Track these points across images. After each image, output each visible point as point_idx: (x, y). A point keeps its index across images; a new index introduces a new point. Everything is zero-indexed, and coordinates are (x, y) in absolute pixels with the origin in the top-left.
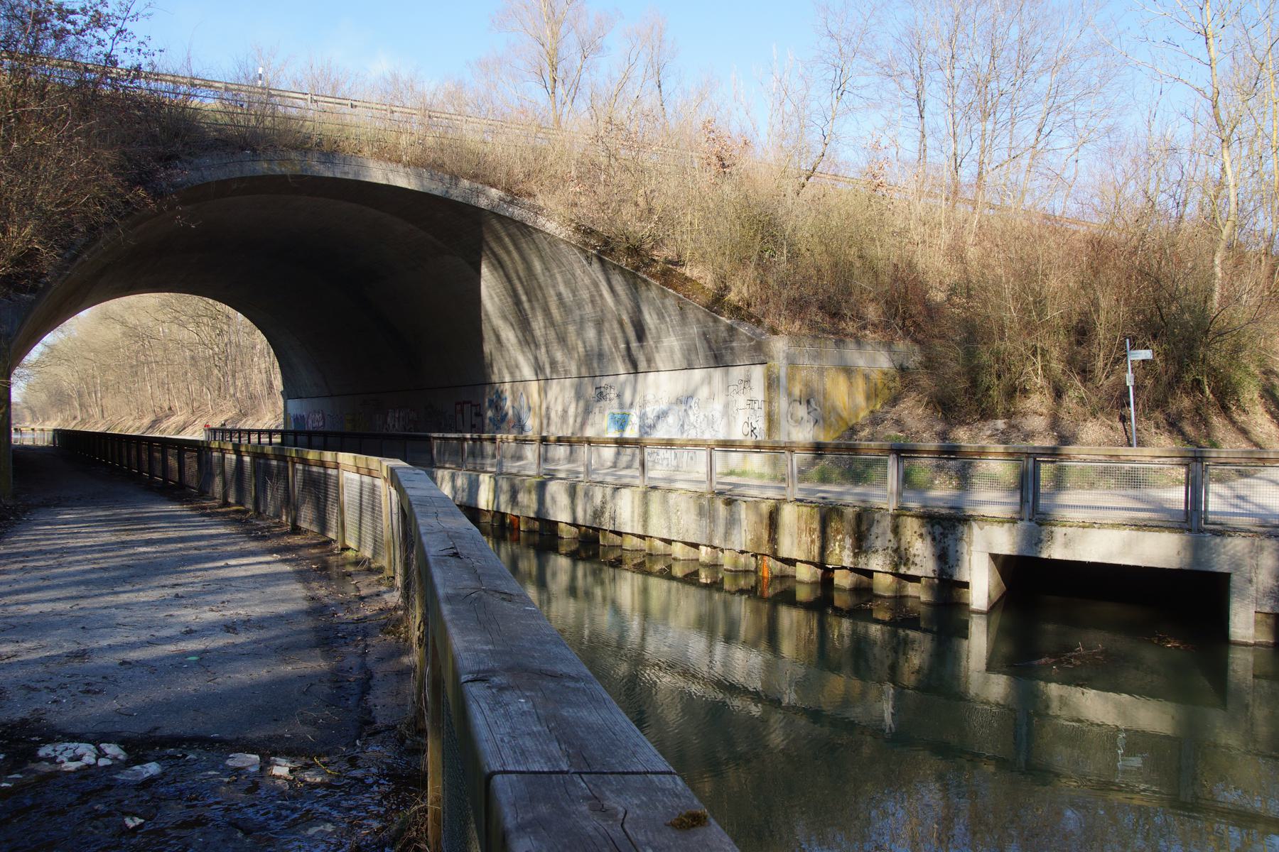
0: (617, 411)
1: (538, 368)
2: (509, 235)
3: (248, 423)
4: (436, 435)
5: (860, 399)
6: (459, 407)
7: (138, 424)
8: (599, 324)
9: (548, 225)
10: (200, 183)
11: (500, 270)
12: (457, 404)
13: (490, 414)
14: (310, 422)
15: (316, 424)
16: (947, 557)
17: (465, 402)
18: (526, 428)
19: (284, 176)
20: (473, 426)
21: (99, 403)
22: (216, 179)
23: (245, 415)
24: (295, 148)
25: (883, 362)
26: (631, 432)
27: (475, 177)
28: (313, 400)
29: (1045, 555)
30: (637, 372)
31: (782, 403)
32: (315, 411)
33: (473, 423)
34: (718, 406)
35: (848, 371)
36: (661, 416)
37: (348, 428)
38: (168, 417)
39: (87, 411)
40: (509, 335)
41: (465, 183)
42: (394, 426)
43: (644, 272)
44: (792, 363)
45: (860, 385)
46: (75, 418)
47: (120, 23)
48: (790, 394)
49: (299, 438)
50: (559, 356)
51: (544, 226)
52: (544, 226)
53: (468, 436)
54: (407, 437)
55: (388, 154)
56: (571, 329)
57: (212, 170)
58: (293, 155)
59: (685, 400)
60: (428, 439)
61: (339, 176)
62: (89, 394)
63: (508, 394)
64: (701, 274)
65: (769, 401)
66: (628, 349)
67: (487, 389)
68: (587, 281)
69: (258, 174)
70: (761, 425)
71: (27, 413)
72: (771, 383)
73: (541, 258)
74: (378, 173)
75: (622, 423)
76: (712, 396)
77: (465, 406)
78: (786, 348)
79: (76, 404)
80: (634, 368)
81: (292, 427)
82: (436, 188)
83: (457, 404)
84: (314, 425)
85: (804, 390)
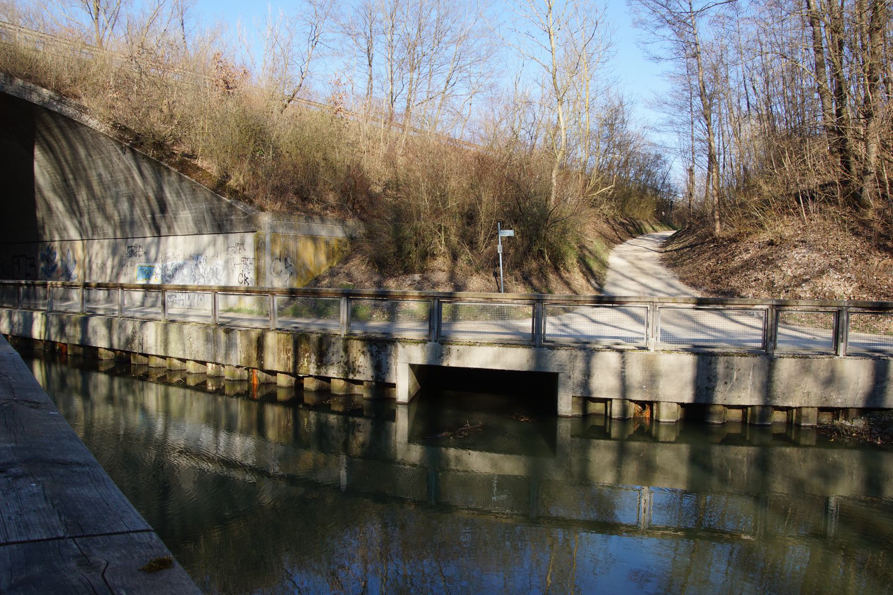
1: (82, 231)
5: (323, 258)
8: (131, 200)
9: (91, 121)
13: (42, 265)
16: (381, 367)
27: (28, 78)
29: (445, 364)
31: (267, 260)
35: (314, 239)
36: (178, 268)
40: (58, 205)
51: (87, 122)
52: (87, 122)
53: (23, 282)
56: (109, 202)
65: (257, 259)
66: (153, 218)
68: (122, 166)
70: (251, 276)
72: (259, 247)
75: (148, 273)
78: (270, 221)
80: (158, 232)
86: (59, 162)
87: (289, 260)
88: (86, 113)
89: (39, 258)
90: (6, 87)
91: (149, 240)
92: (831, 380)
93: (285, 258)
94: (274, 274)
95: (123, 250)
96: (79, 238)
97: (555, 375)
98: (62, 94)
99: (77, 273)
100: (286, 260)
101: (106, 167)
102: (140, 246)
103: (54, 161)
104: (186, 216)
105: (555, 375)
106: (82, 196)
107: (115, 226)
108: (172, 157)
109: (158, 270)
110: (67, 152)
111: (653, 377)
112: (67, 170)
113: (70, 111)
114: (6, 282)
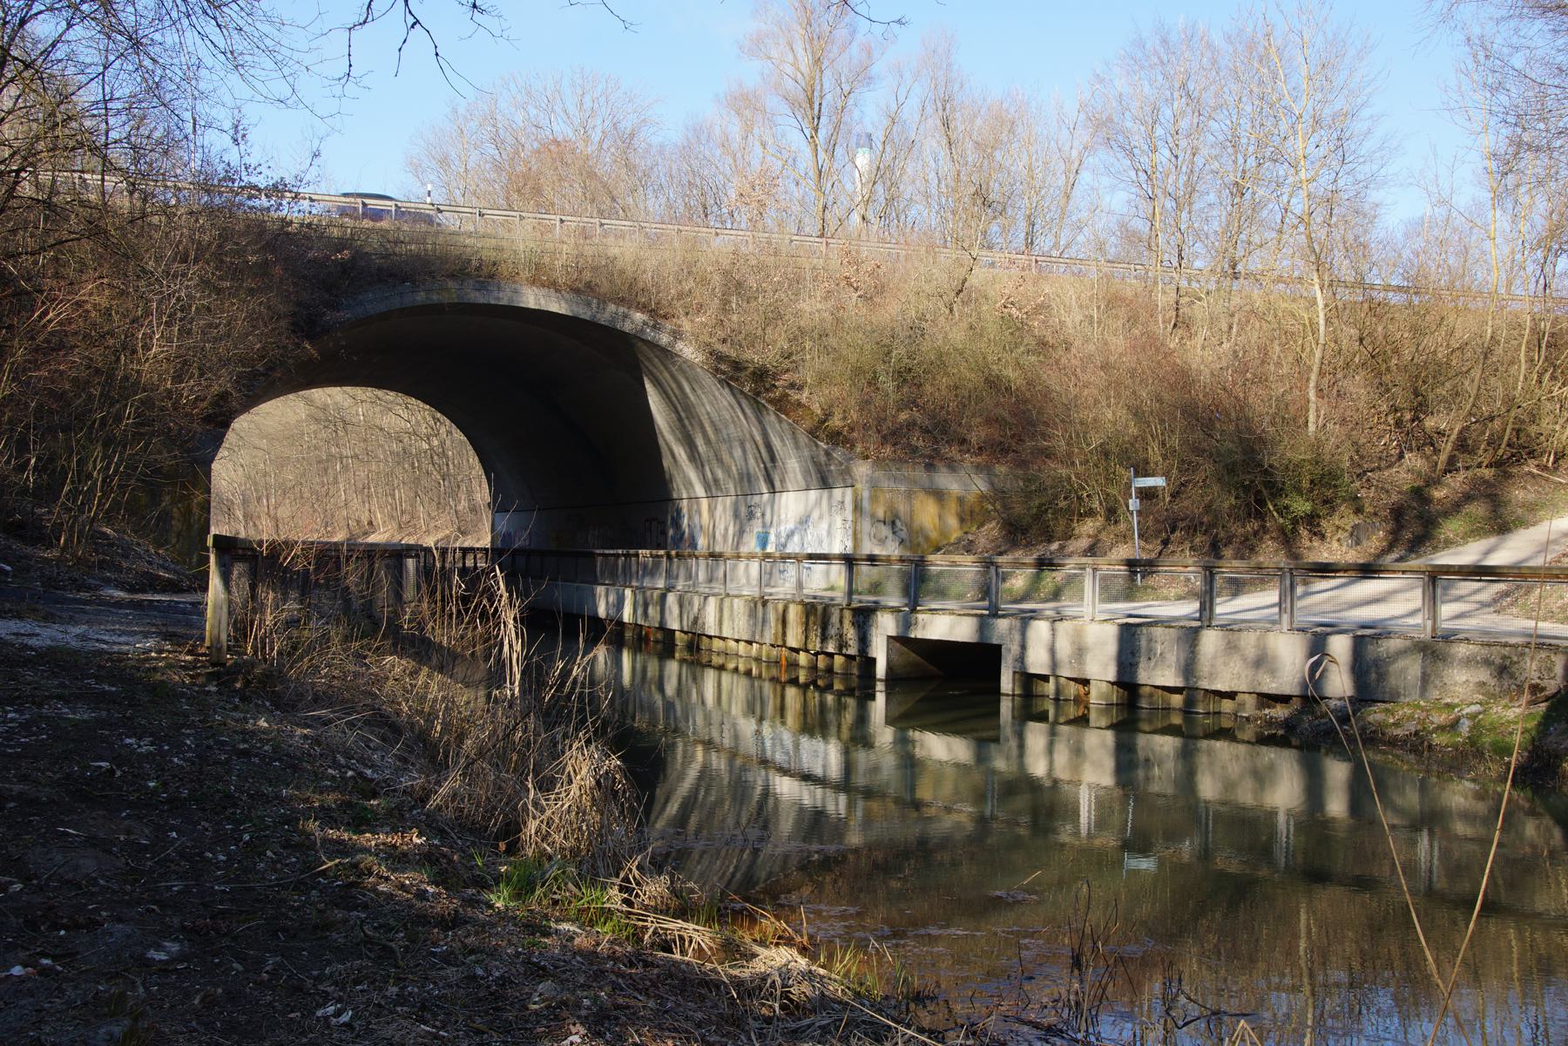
0: (760, 529)
1: (707, 487)
2: (657, 357)
4: (598, 551)
5: (953, 522)
9: (685, 349)
13: (671, 532)
16: (864, 641)
19: (442, 305)
21: (272, 513)
24: (452, 276)
25: (980, 485)
27: (622, 301)
29: (913, 636)
31: (866, 525)
34: (824, 525)
35: (939, 495)
36: (790, 535)
39: (255, 525)
40: (681, 452)
41: (612, 307)
44: (874, 486)
45: (953, 506)
47: (295, 190)
48: (873, 516)
50: (720, 474)
53: (620, 551)
55: (541, 277)
56: (724, 447)
57: (375, 302)
58: (451, 284)
59: (804, 521)
60: (593, 555)
61: (493, 302)
62: (259, 499)
63: (685, 511)
64: (813, 400)
65: (855, 522)
66: (766, 468)
67: (670, 504)
68: (726, 403)
70: (850, 544)
72: (857, 508)
73: (687, 379)
74: (532, 299)
75: (764, 542)
76: (821, 517)
78: (870, 472)
79: (240, 514)
80: (773, 490)
81: (499, 544)
82: (584, 313)
85: (888, 514)
86: (665, 392)
87: (898, 523)
90: (598, 316)
91: (766, 496)
92: (1262, 661)
93: (892, 522)
94: (875, 541)
96: (704, 495)
97: (999, 647)
98: (657, 314)
99: (702, 542)
100: (893, 523)
101: (711, 404)
104: (793, 465)
105: (999, 647)
108: (772, 391)
109: (772, 538)
110: (674, 386)
111: (1080, 652)
112: (680, 409)
113: (664, 339)
114: (607, 552)
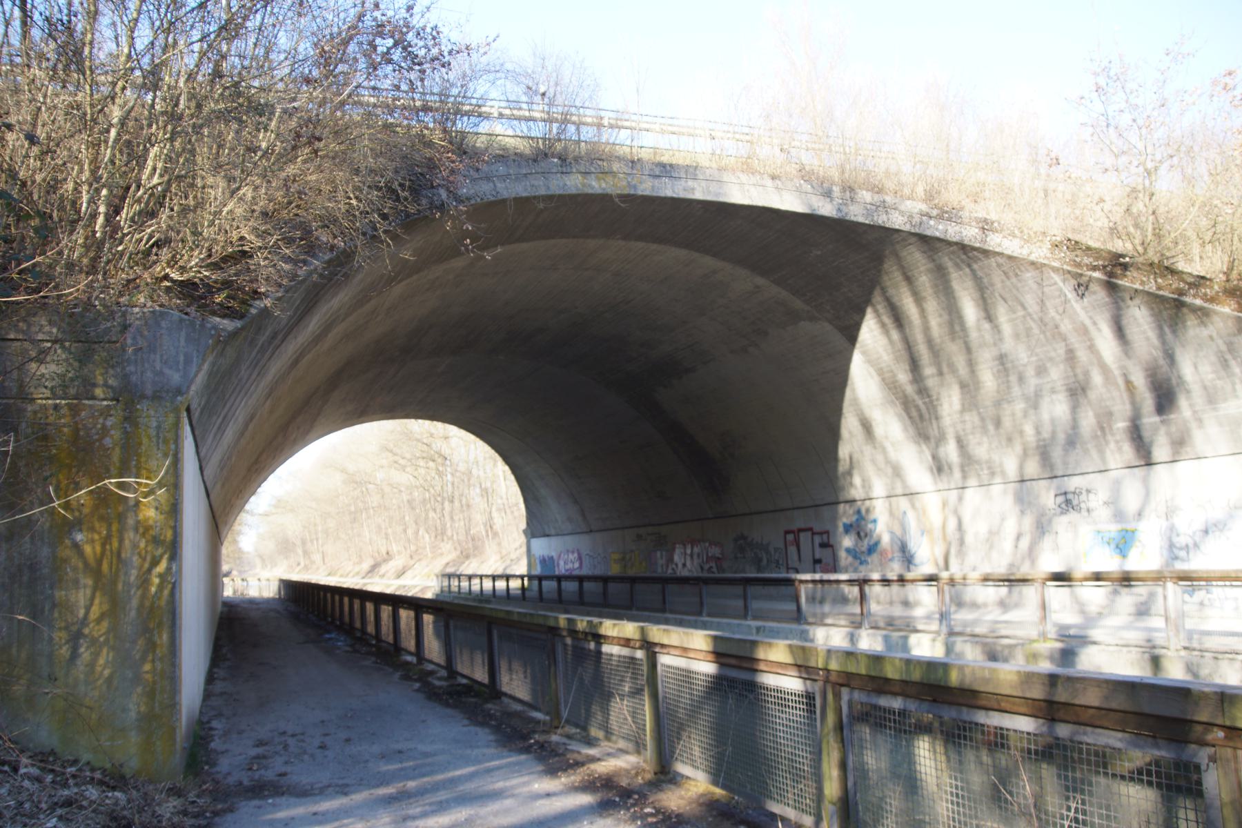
3: (472, 565)
6: (790, 537)
7: (357, 569)
8: (1077, 391)
10: (492, 199)
11: (895, 335)
12: (787, 532)
13: (847, 542)
14: (562, 563)
15: (570, 566)
17: (800, 530)
18: (917, 560)
20: (817, 561)
21: (321, 550)
22: (513, 195)
23: (467, 557)
26: (1142, 559)
28: (567, 538)
30: (1149, 464)
32: (568, 551)
33: (817, 556)
37: (615, 570)
38: (385, 561)
42: (684, 565)
43: (1194, 296)
46: (299, 564)
49: (544, 583)
51: (1000, 245)
52: (1000, 245)
54: (706, 581)
62: (312, 541)
69: (569, 192)
71: (258, 561)
75: (1123, 544)
77: (802, 535)
79: (300, 551)
80: (1144, 455)
81: (537, 571)
82: (826, 209)
83: (787, 532)
84: (567, 567)
88: (994, 231)
89: (841, 529)
95: (1047, 497)
102: (1088, 491)
103: (910, 340)
106: (950, 402)
107: (1025, 452)
